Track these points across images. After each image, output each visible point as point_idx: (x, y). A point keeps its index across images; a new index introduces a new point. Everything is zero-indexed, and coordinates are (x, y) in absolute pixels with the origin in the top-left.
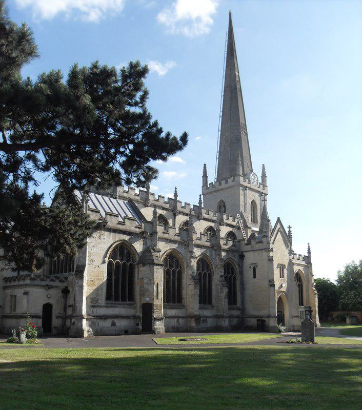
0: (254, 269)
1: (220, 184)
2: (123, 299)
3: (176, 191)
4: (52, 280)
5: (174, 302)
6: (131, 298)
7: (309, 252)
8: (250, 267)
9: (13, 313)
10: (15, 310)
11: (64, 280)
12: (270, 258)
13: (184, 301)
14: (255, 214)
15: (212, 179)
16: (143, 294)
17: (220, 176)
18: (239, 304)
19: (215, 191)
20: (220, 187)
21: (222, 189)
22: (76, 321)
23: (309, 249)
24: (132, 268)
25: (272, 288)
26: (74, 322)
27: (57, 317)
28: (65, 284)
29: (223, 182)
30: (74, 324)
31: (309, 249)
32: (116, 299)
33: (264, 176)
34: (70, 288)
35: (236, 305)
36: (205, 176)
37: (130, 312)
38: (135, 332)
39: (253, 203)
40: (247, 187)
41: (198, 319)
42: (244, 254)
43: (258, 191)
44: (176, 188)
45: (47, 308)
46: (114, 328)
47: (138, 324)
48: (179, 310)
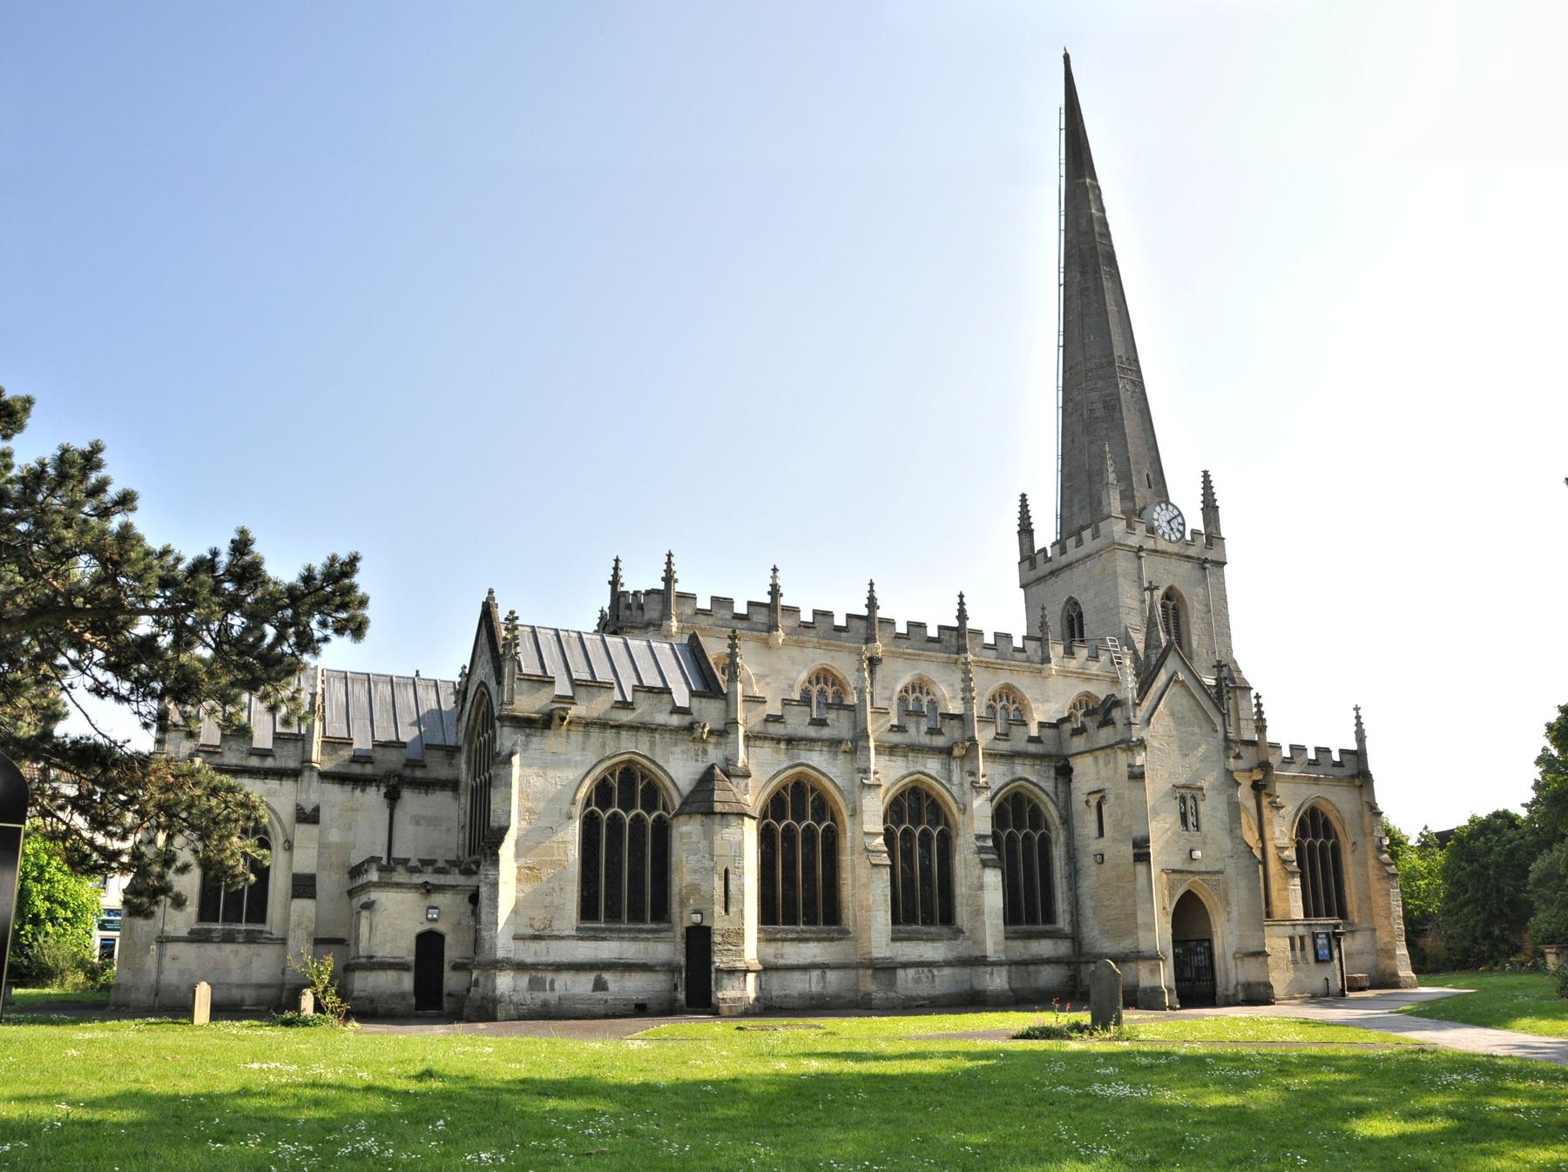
1: (1063, 551)
2: (637, 915)
6: (661, 912)
7: (1360, 736)
8: (1087, 802)
12: (1136, 770)
13: (849, 914)
14: (1183, 628)
15: (1046, 534)
17: (1069, 529)
18: (1063, 922)
19: (1052, 573)
20: (1064, 560)
21: (1069, 566)
22: (481, 979)
23: (1359, 724)
24: (662, 831)
25: (1141, 868)
26: (477, 980)
27: (457, 967)
29: (1071, 542)
30: (476, 983)
31: (1359, 724)
32: (614, 915)
33: (1210, 508)
35: (1055, 923)
36: (1026, 530)
38: (669, 1010)
41: (886, 969)
43: (1188, 557)
45: (429, 944)
46: (599, 995)
48: (826, 944)
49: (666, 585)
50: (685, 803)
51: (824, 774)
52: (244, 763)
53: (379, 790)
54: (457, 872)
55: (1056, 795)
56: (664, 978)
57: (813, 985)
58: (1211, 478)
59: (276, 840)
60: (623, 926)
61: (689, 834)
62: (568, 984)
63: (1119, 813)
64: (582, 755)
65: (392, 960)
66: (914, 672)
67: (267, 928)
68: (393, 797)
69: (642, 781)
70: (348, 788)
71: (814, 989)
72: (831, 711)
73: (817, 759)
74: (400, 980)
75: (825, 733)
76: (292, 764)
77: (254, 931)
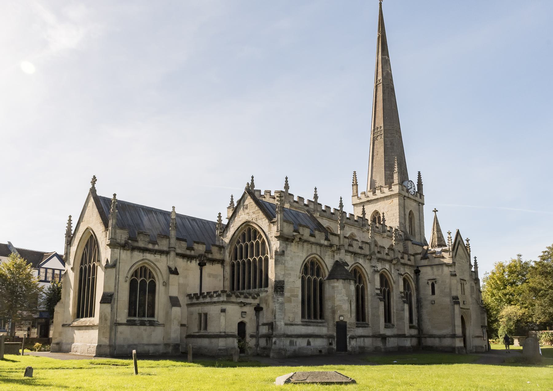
0: (433, 286)
3: (341, 201)
4: (246, 297)
5: (315, 318)
8: (428, 283)
9: (203, 332)
10: (206, 328)
11: (256, 296)
16: (334, 312)
24: (321, 284)
27: (252, 336)
28: (256, 302)
34: (263, 305)
36: (355, 184)
37: (324, 331)
39: (411, 213)
40: (405, 196)
42: (420, 269)
44: (287, 178)
45: (242, 326)
47: (331, 344)
49: (286, 190)
50: (330, 275)
51: (363, 267)
52: (147, 247)
53: (196, 262)
54: (251, 298)
55: (414, 279)
56: (325, 340)
57: (362, 344)
58: (421, 174)
59: (159, 281)
60: (317, 321)
61: (337, 287)
62: (300, 343)
63: (443, 287)
64: (302, 254)
65: (231, 334)
66: (351, 232)
67: (155, 319)
68: (202, 265)
69: (316, 265)
70: (185, 260)
71: (362, 345)
72: (364, 244)
73: (361, 261)
74: (234, 342)
75: (362, 252)
76: (165, 248)
77: (151, 321)
